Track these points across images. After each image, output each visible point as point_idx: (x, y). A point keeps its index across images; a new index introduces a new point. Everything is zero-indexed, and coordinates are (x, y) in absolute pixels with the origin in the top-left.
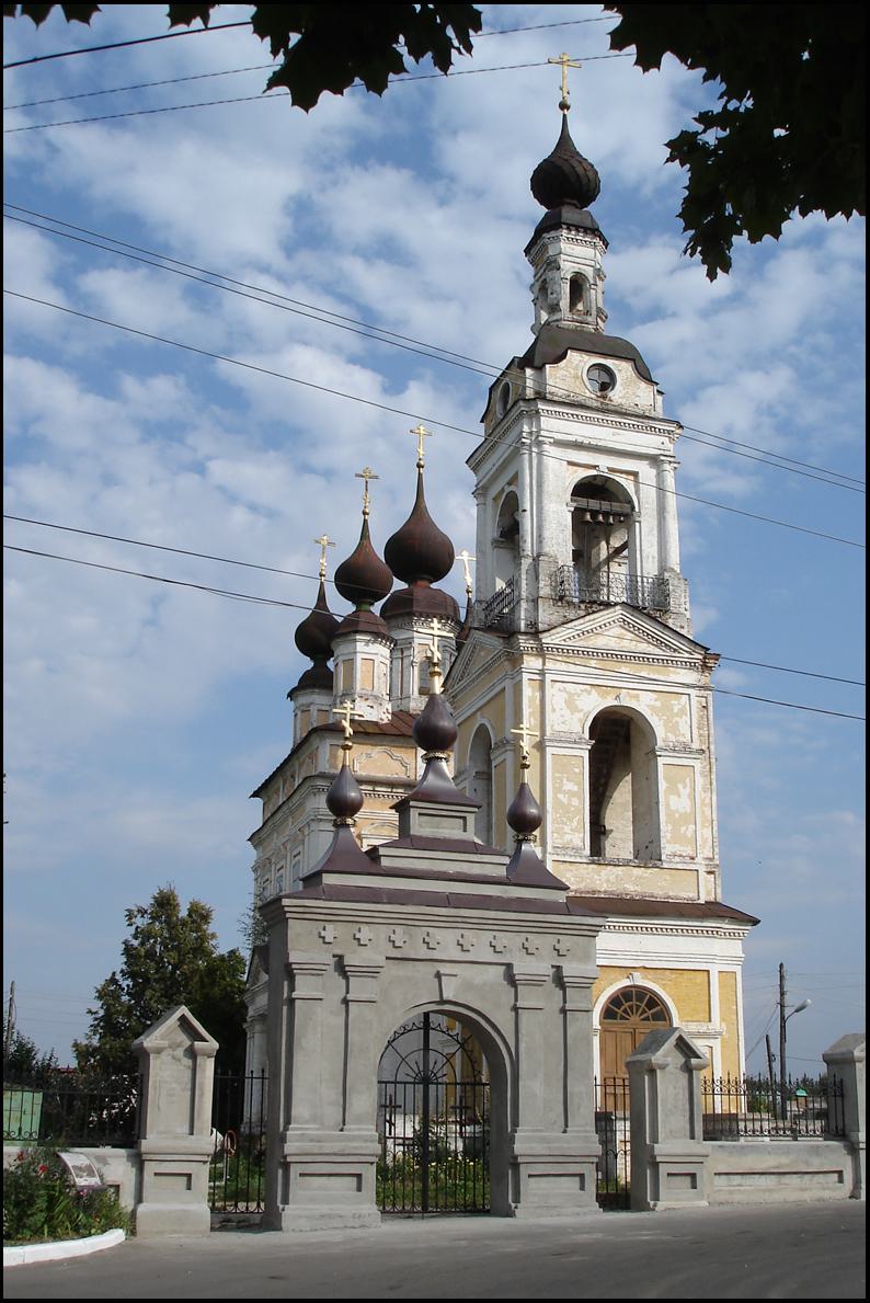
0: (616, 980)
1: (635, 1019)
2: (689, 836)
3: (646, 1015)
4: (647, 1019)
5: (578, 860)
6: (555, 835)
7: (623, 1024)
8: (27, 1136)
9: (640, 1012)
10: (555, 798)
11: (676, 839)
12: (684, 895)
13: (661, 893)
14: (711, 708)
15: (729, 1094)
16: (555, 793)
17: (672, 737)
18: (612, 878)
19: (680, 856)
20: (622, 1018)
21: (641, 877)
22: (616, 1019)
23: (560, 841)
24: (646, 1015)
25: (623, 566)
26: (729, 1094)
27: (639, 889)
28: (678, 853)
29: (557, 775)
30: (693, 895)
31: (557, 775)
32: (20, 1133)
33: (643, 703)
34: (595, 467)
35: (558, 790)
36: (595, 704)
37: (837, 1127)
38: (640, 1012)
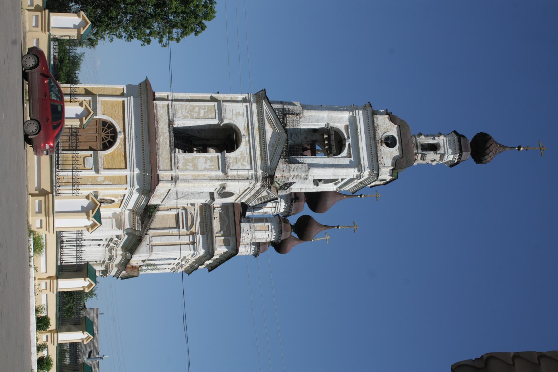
0: (119, 126)
1: (103, 135)
2: (187, 167)
3: (107, 132)
4: (103, 140)
5: (170, 115)
6: (180, 106)
7: (100, 129)
8: (57, 174)
9: (106, 132)
10: (197, 106)
11: (186, 161)
12: (161, 163)
13: (160, 153)
14: (277, 129)
15: (77, 236)
16: (198, 106)
17: (231, 161)
18: (164, 131)
19: (178, 163)
20: (103, 129)
21: (166, 144)
22: (102, 126)
23: (178, 107)
24: (107, 132)
25: (290, 166)
26: (77, 251)
27: (161, 143)
28: (180, 162)
29: (206, 107)
30: (161, 168)
31: (206, 107)
32: (58, 179)
33: (243, 148)
34: (348, 137)
35: (200, 107)
36: (241, 125)
37: (64, 236)
38: (106, 132)
